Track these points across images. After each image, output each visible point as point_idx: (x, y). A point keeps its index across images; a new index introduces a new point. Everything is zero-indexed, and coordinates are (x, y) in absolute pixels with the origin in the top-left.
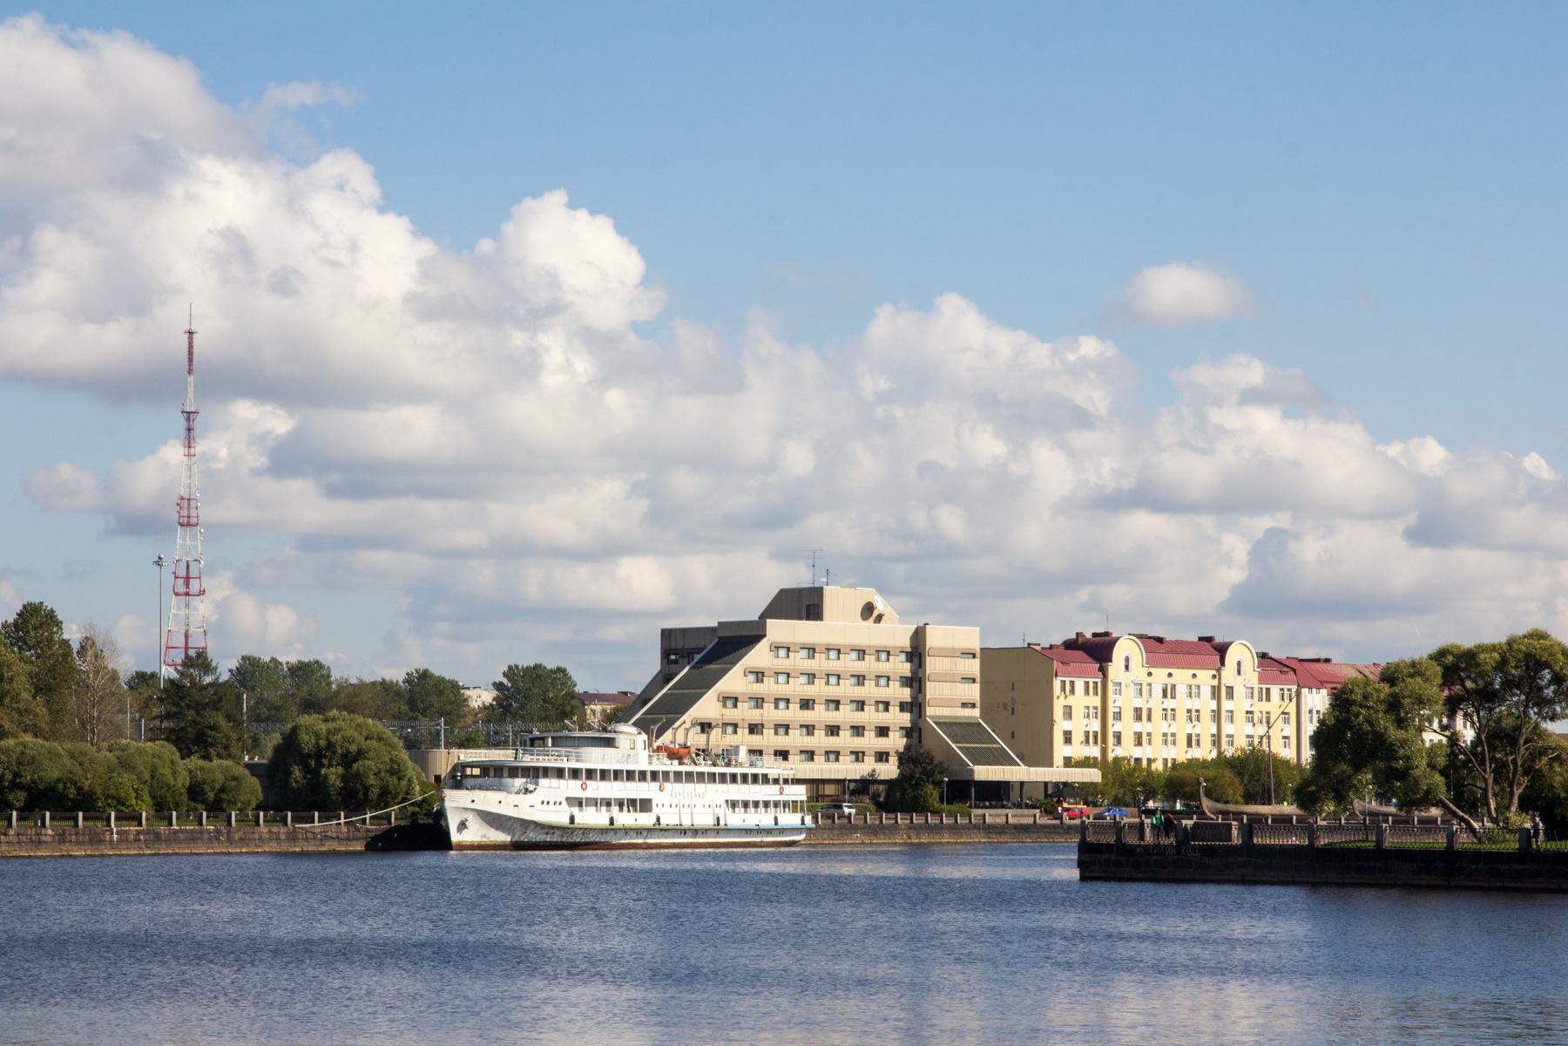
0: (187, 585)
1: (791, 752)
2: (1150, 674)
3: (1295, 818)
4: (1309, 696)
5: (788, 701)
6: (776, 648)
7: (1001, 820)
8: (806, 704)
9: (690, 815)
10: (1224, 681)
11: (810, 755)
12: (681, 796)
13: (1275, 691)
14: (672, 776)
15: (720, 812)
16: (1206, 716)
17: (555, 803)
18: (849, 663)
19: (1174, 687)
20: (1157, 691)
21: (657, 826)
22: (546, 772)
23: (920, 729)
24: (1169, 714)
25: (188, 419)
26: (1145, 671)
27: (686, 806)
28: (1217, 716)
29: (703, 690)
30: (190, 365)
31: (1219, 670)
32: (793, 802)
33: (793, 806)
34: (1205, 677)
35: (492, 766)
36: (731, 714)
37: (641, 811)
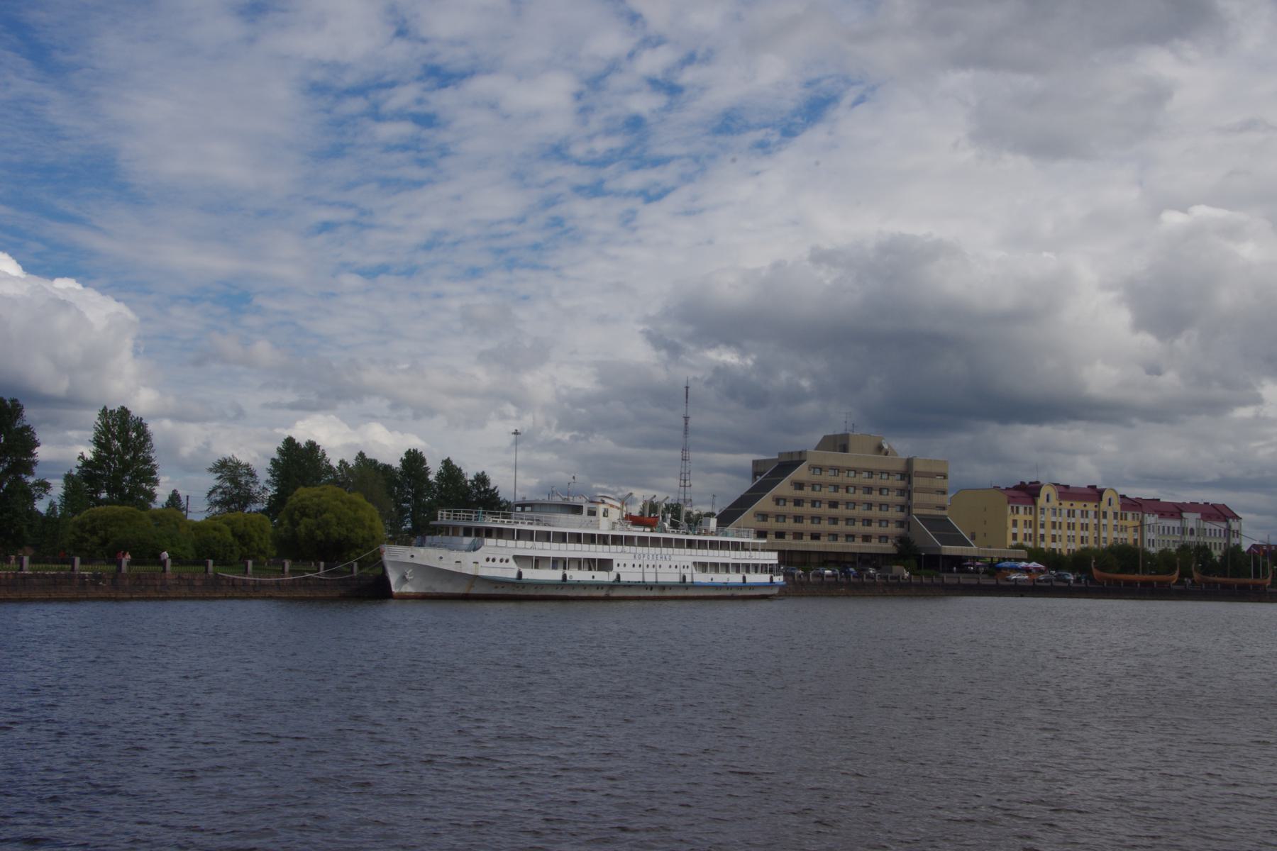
0: (685, 482)
2: (1061, 504)
3: (1122, 583)
4: (1148, 518)
5: (820, 502)
6: (813, 468)
7: (955, 581)
9: (655, 574)
10: (1101, 508)
11: (835, 536)
12: (646, 558)
13: (1130, 515)
14: (636, 540)
15: (687, 572)
16: (1091, 527)
18: (863, 479)
19: (1074, 511)
20: (1065, 512)
21: (617, 583)
22: (489, 533)
23: (909, 523)
24: (1071, 526)
25: (686, 420)
26: (1058, 503)
27: (651, 566)
28: (1097, 527)
29: (762, 493)
31: (1099, 503)
32: (770, 565)
33: (764, 568)
34: (1091, 507)
36: (781, 509)
37: (599, 570)
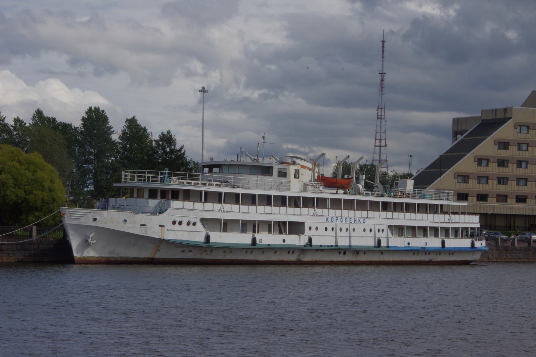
1: (470, 195)
5: (488, 160)
8: (502, 163)
12: (339, 221)
14: (329, 202)
15: (382, 236)
17: (188, 224)
21: (308, 247)
22: (175, 195)
25: (382, 77)
27: (344, 230)
30: (383, 54)
33: (465, 232)
35: (135, 187)
37: (224, 231)
